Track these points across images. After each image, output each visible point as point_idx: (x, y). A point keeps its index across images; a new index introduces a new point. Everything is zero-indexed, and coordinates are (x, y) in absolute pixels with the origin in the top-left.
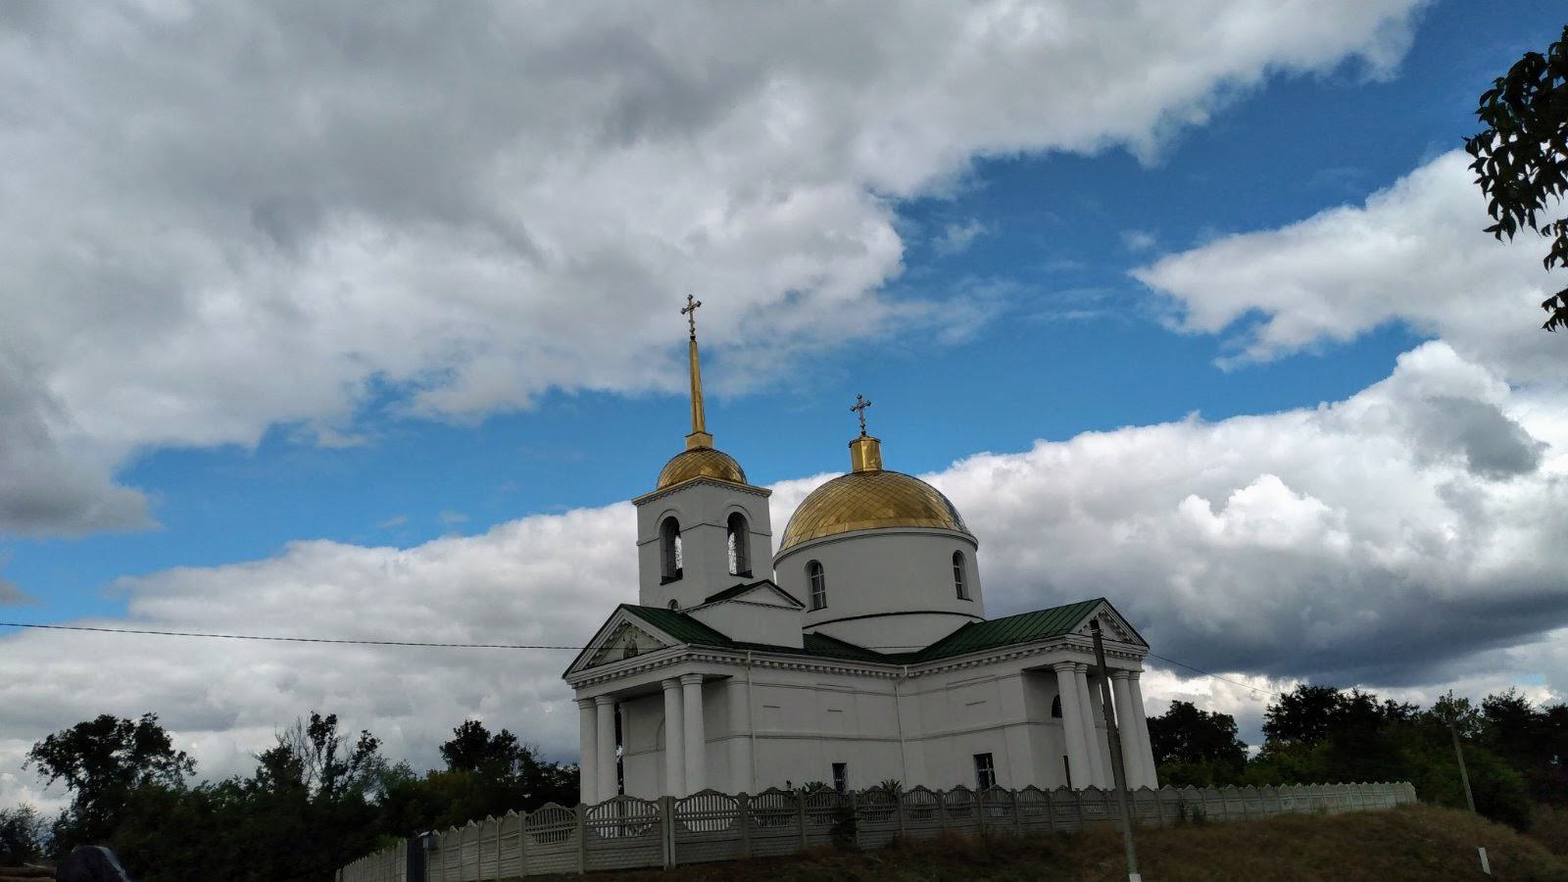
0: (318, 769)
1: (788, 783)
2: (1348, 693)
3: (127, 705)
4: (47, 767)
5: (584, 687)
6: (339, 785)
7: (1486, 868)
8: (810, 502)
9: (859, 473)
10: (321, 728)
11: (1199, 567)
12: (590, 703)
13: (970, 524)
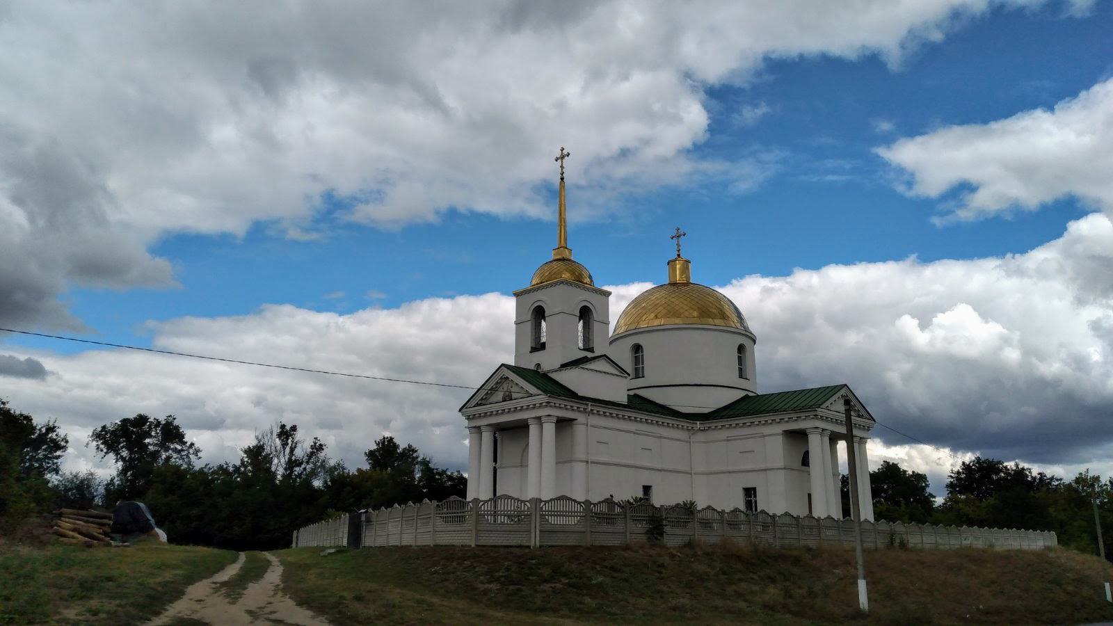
0: (283, 460)
1: (612, 496)
2: (1010, 465)
3: (155, 409)
4: (102, 446)
6: (296, 473)
8: (637, 302)
9: (674, 284)
10: (286, 433)
11: (907, 366)
12: (478, 429)
13: (753, 326)
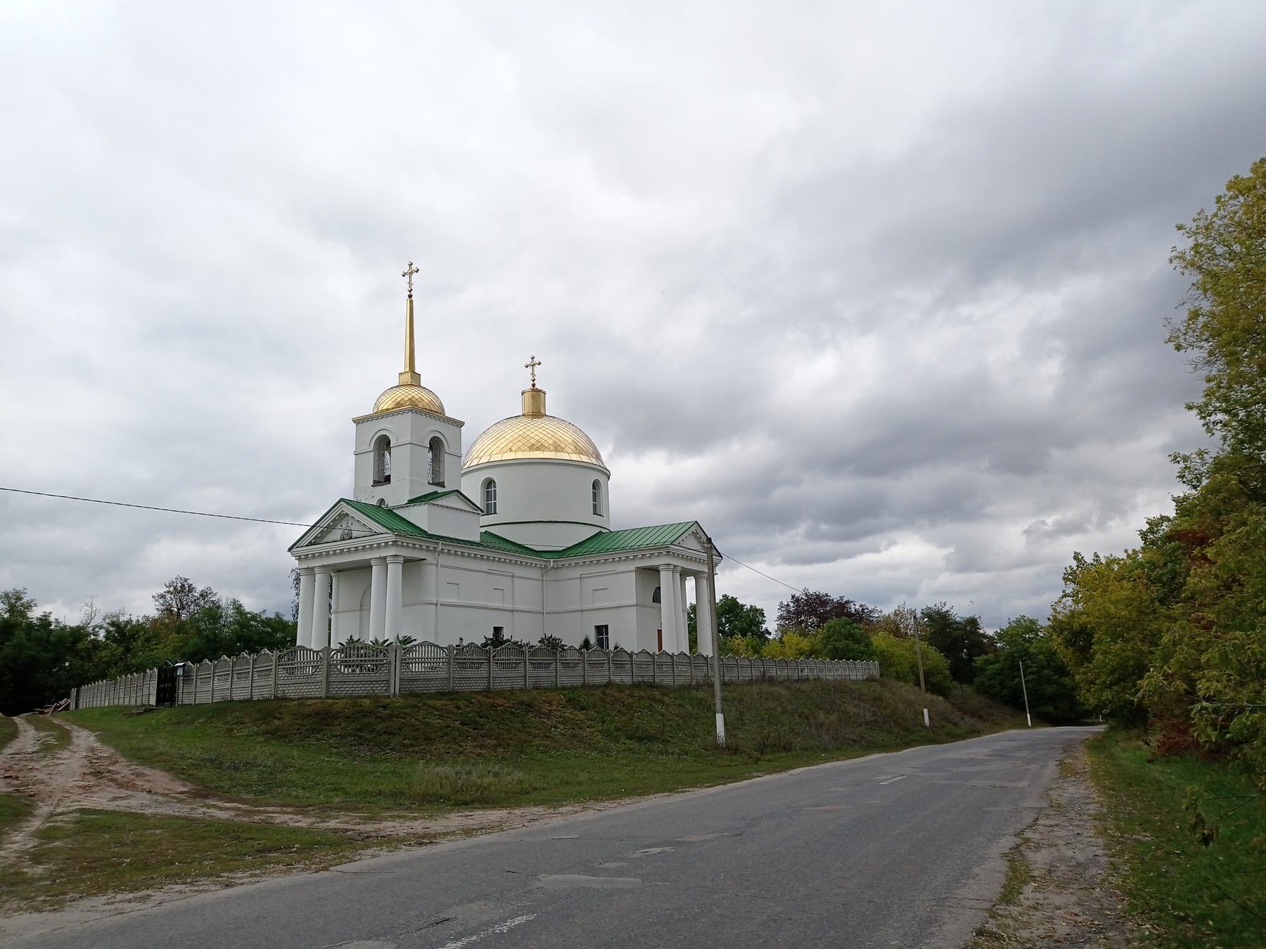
7: (926, 711)
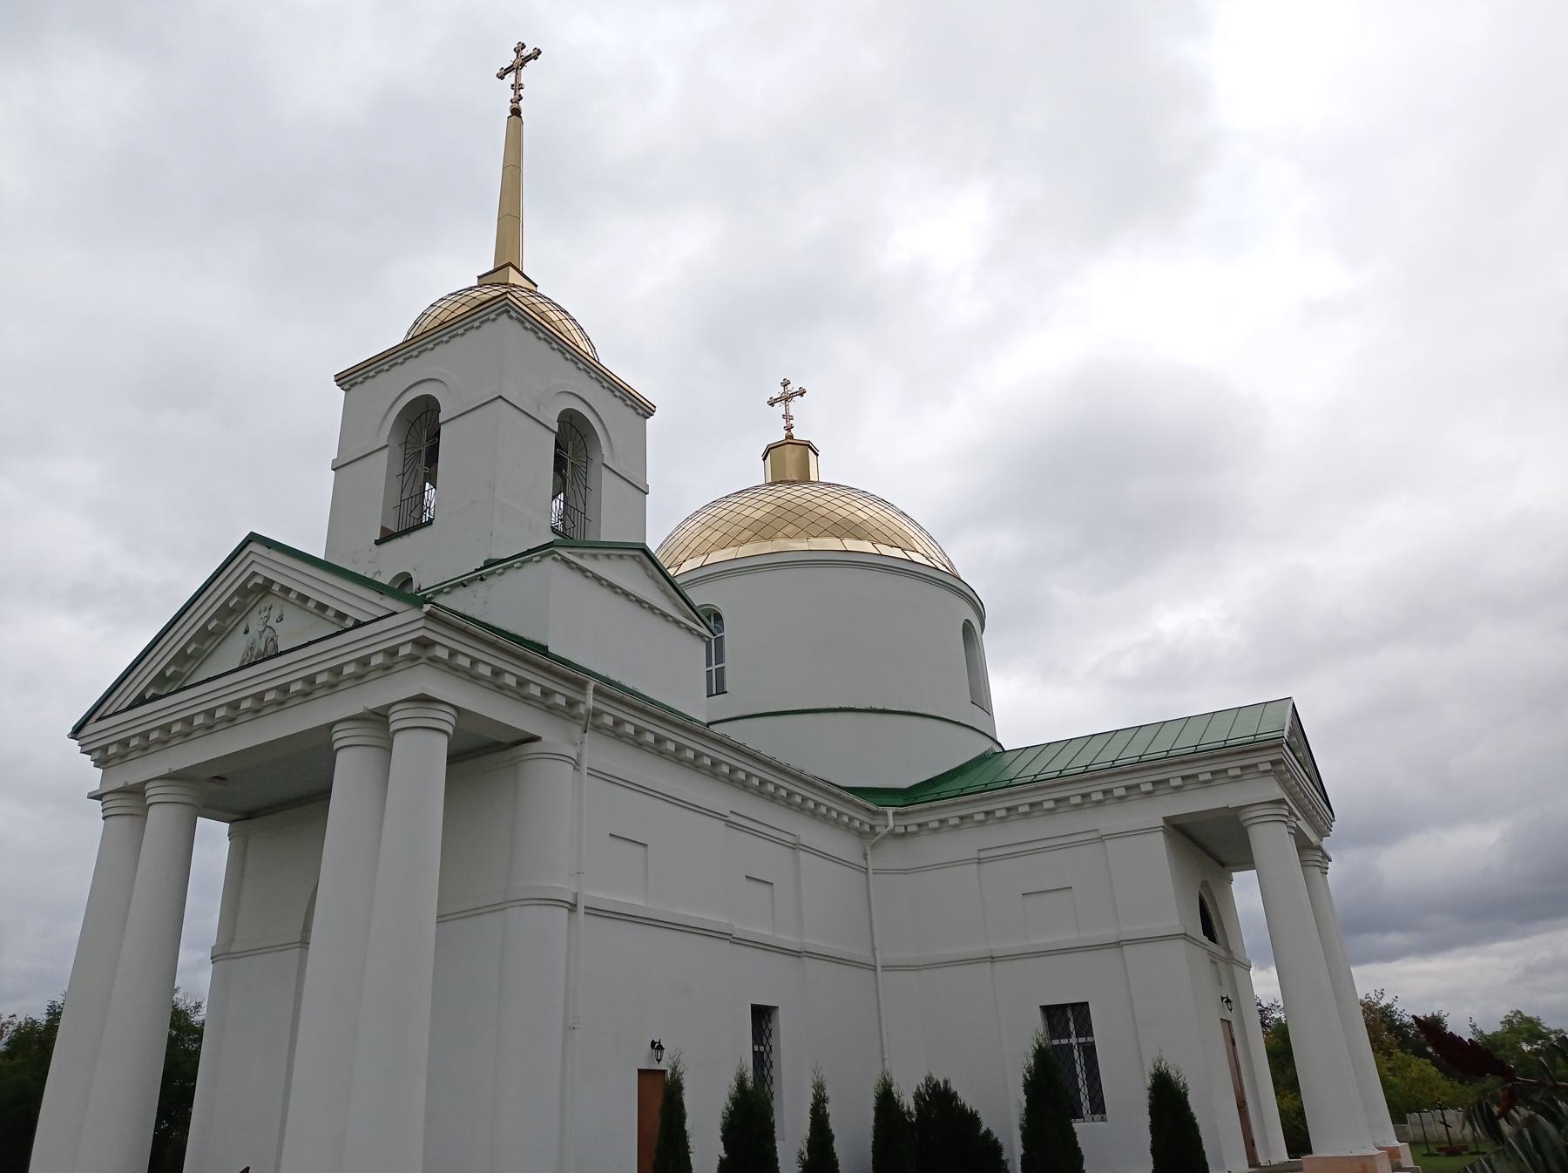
1: (657, 1047)
5: (122, 758)
